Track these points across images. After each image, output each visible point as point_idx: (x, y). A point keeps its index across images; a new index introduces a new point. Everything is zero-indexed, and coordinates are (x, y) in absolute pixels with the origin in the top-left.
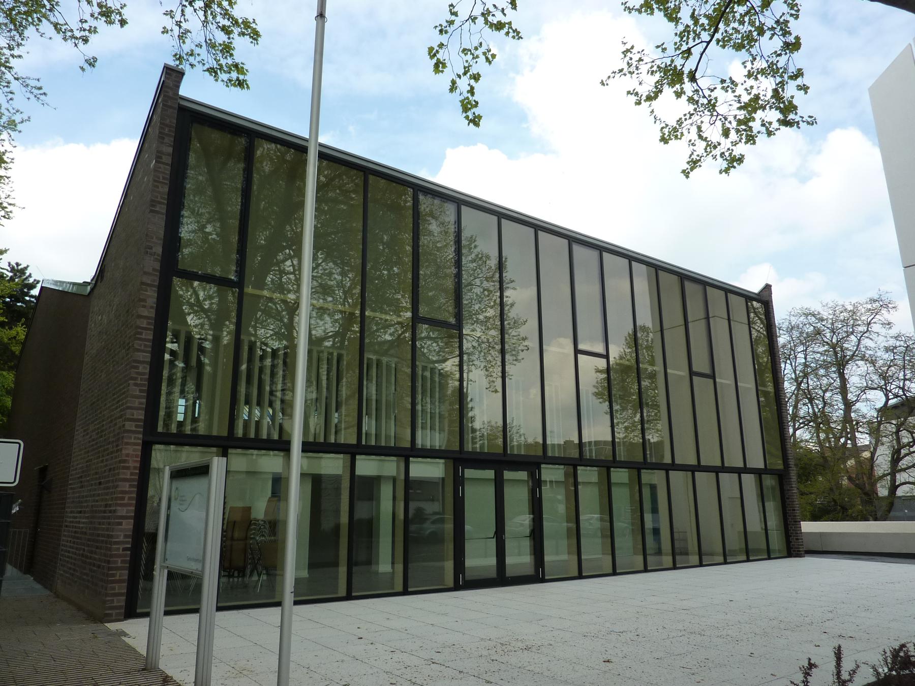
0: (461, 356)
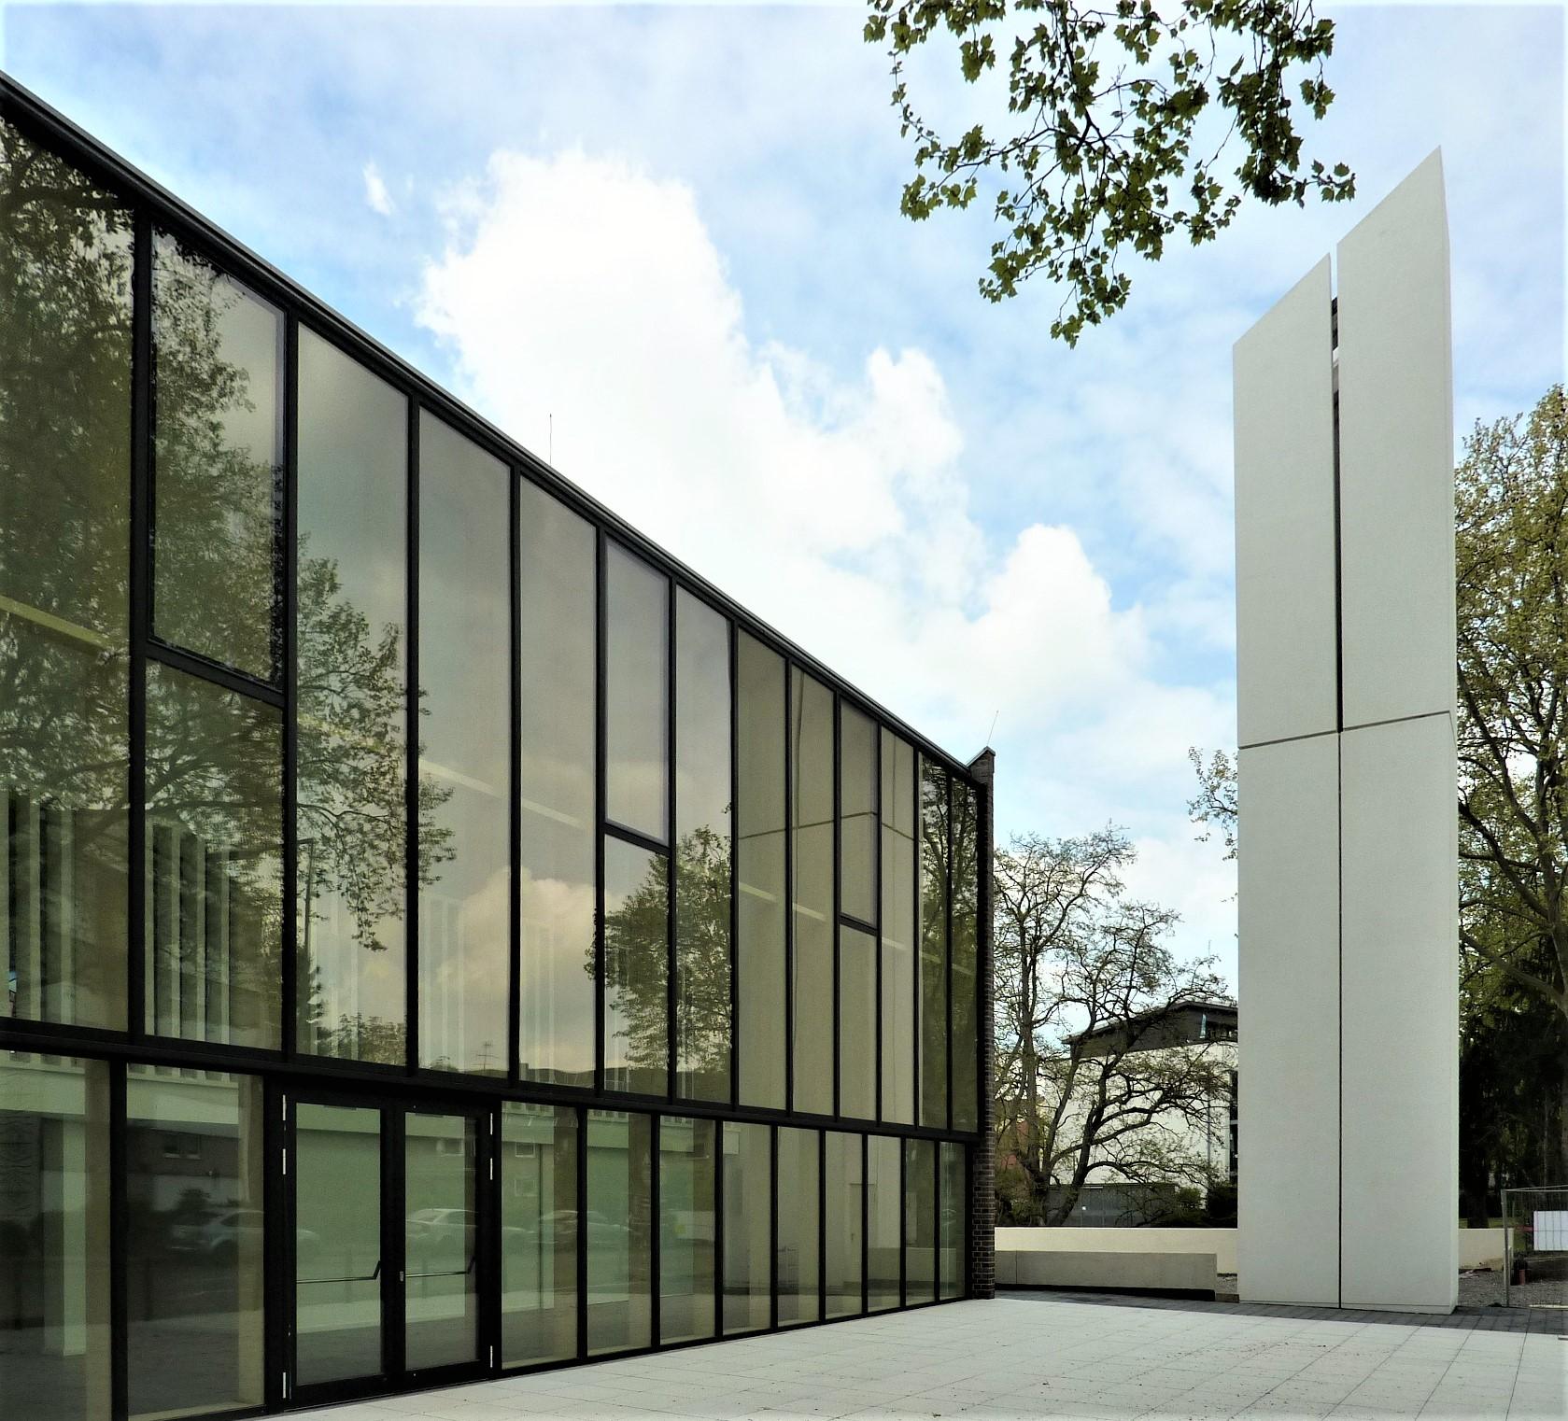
0: (289, 853)
